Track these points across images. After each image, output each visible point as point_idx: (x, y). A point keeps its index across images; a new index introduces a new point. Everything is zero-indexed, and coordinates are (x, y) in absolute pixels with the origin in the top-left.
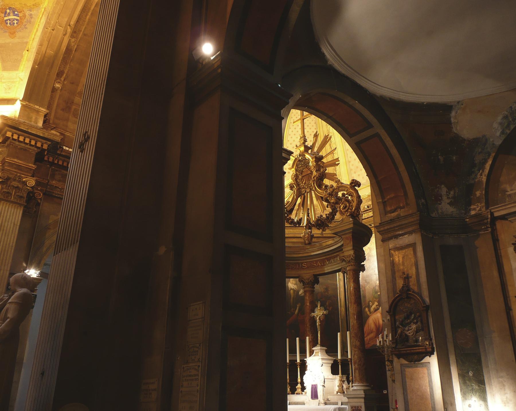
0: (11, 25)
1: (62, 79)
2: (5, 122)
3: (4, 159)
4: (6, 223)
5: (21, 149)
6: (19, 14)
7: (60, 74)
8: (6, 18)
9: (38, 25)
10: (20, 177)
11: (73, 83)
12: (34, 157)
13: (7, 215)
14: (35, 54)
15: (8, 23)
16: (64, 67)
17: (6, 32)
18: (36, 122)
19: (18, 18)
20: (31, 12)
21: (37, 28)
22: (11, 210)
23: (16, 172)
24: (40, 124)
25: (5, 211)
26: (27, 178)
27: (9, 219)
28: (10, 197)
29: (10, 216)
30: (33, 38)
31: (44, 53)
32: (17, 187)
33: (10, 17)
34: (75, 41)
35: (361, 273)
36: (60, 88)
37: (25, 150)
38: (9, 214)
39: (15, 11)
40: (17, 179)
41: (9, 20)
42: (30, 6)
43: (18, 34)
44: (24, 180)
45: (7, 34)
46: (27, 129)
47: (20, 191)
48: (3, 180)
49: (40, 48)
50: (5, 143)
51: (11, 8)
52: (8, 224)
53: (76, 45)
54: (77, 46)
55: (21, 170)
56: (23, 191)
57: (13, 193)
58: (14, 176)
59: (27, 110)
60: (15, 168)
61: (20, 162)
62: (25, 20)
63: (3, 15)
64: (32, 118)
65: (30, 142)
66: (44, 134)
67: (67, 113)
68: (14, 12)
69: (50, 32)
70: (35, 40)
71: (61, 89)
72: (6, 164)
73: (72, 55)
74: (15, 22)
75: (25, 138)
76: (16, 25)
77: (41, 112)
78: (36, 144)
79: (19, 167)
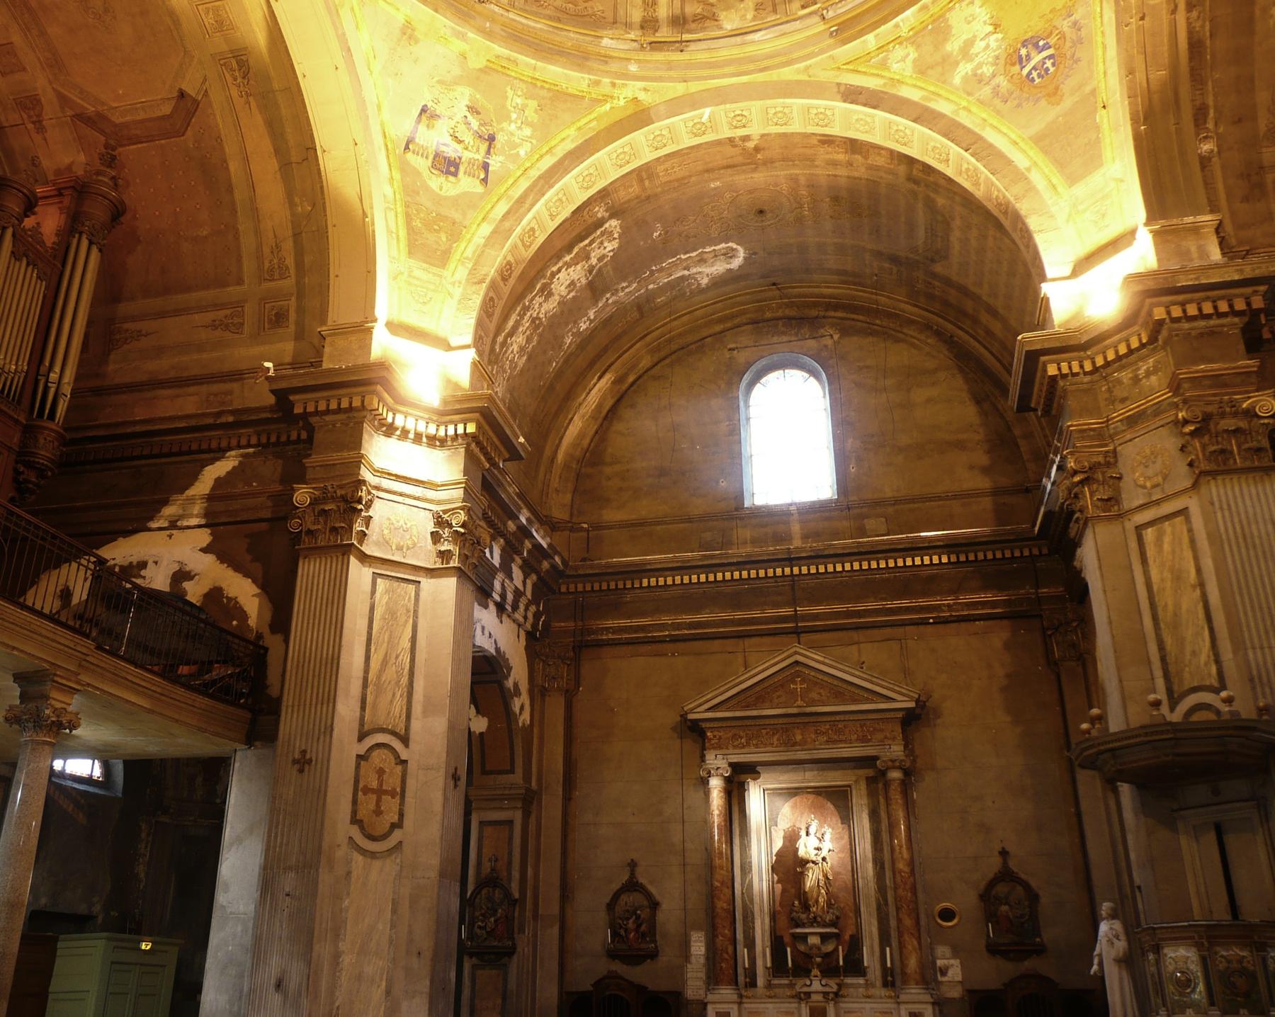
0: (1043, 77)
1: (1210, 125)
2: (1140, 288)
3: (1174, 375)
4: (1254, 527)
5: (1201, 335)
6: (1049, 40)
7: (1200, 115)
8: (1025, 71)
9: (1100, 34)
10: (1233, 404)
11: (1240, 120)
12: (1242, 341)
13: (1245, 507)
14: (1127, 102)
15: (1036, 78)
16: (1202, 94)
17: (1038, 100)
18: (1203, 253)
19: (1050, 51)
20: (1073, 18)
21: (410, 926)
22: (1250, 491)
23: (1214, 395)
24: (1216, 255)
25: (1235, 497)
26: (1249, 398)
27: (1255, 514)
28: (1231, 461)
29: (1254, 507)
30: (1102, 71)
31: (1145, 85)
32: (1237, 431)
33: (1032, 63)
34: (1200, 13)
35: (188, 598)
36: (1216, 149)
37: (1211, 333)
38: (1248, 502)
39: (1038, 42)
40: (1228, 410)
41: (1034, 68)
42: (1064, 7)
43: (1066, 88)
44: (1245, 405)
45: (1043, 103)
46: (1197, 279)
47: (1249, 436)
48: (1198, 426)
49: (1131, 81)
50: (1156, 340)
51: (1026, 41)
52: (1259, 530)
53: (1207, 23)
54: (1211, 21)
55: (1226, 385)
56: (1254, 434)
57: (1235, 448)
58: (1216, 406)
59: (1169, 238)
60: (1211, 387)
61: (1215, 366)
62: (1068, 44)
63: (1017, 67)
64: (1188, 252)
65: (1215, 308)
66: (1241, 271)
67: (1259, 200)
68: (1036, 45)
69: (1138, 28)
70: (1110, 72)
71: (1219, 152)
72: (1186, 386)
73: (1208, 50)
74: (1049, 64)
75: (1199, 304)
76: (1052, 69)
77: (1203, 227)
78: (1231, 306)
79: (1217, 381)
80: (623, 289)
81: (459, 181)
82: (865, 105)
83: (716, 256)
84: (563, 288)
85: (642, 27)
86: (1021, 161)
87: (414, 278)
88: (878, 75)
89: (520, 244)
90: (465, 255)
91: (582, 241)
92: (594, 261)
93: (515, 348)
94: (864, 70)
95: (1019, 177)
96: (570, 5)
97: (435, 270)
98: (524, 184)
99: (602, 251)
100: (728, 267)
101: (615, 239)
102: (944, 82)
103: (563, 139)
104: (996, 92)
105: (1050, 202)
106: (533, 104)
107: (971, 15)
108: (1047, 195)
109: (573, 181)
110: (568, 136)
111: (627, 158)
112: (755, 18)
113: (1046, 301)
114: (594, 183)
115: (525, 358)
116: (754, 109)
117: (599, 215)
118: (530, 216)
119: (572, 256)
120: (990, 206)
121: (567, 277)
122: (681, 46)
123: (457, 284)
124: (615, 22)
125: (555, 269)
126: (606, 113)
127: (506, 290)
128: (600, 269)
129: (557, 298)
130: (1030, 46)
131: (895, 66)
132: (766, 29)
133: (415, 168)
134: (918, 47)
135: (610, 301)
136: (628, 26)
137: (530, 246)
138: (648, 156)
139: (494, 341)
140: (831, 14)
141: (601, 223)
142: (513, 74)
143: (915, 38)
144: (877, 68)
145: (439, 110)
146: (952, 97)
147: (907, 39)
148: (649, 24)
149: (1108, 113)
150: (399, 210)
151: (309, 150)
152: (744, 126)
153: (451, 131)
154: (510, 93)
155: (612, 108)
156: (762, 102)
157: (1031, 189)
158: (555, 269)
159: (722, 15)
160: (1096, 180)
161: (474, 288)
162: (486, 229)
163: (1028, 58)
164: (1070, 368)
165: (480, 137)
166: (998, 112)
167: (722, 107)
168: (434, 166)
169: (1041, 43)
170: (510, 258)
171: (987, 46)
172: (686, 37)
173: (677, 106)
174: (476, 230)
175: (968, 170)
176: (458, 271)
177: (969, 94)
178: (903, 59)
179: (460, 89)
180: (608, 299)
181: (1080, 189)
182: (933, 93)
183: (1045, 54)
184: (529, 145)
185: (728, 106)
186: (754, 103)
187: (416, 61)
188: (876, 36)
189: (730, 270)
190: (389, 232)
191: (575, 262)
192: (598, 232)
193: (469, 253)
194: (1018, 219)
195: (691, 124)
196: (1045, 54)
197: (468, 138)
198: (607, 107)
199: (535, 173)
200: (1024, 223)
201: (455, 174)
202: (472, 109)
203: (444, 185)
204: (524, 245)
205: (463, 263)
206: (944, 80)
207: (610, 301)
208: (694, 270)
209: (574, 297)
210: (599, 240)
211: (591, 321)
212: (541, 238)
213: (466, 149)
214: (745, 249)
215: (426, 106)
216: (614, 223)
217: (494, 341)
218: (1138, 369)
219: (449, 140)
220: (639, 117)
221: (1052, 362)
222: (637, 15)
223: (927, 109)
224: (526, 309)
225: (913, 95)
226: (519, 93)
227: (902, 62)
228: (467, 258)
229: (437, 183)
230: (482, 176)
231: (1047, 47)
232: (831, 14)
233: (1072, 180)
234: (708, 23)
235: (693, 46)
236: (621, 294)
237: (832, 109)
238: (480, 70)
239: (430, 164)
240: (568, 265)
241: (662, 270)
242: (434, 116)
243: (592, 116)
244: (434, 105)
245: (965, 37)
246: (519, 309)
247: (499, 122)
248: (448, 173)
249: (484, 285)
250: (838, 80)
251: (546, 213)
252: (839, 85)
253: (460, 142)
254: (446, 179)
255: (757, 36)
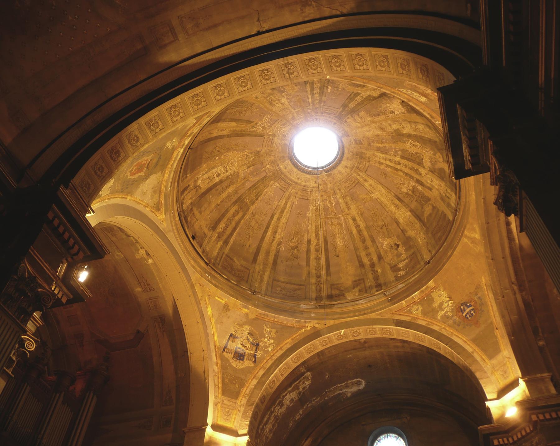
8: (464, 315)
18: (548, 391)
20: (478, 296)
24: (553, 391)
30: (493, 315)
33: (467, 311)
36: (545, 344)
39: (467, 304)
41: (467, 313)
51: (462, 303)
63: (461, 313)
68: (466, 305)
74: (472, 312)
76: (474, 314)
80: (314, 400)
81: (244, 362)
82: (404, 327)
83: (353, 384)
84: (288, 402)
85: (316, 300)
86: (469, 348)
87: (225, 404)
88: (408, 316)
89: (269, 387)
90: (246, 393)
91: (295, 382)
92: (301, 389)
93: (268, 430)
94: (403, 314)
95: (470, 356)
96: (288, 293)
97: (233, 400)
98: (271, 362)
99: (304, 385)
100: (359, 388)
101: (309, 380)
102: (434, 318)
103: (286, 344)
104: (454, 322)
105: (483, 366)
106: (274, 331)
107: (440, 294)
108: (482, 363)
109: (290, 360)
110: (288, 342)
111: (312, 350)
112: (359, 295)
113: (488, 409)
114: (299, 360)
115: (272, 434)
116: (361, 329)
117: (302, 371)
118: (273, 375)
119: (291, 388)
120: (461, 367)
121: (290, 397)
122: (331, 306)
123: (242, 406)
124: (305, 298)
125: (284, 394)
126: (303, 333)
127: (263, 407)
128: (304, 393)
129: (285, 406)
130: (464, 305)
131: (414, 312)
132: (363, 299)
133: (226, 358)
134: (422, 306)
135: (309, 406)
136: (311, 299)
137: (273, 388)
138: (321, 348)
139: (258, 428)
140: (388, 293)
141: (303, 374)
142: (266, 320)
143: (421, 302)
144: (407, 313)
145: (237, 335)
146: (438, 324)
147: (418, 303)
148: (319, 298)
149: (498, 331)
150: (219, 376)
151: (185, 352)
152: (358, 336)
153: (242, 343)
154: (265, 327)
155: (305, 331)
156: (364, 327)
157: (475, 360)
158: (284, 394)
159: (347, 294)
160: (500, 357)
161: (249, 408)
162: (255, 382)
163: (465, 310)
164: (503, 441)
165: (253, 344)
166: (457, 330)
167: (348, 329)
168: (234, 357)
169: (468, 304)
170: (264, 393)
171: (448, 305)
172: (333, 303)
173: (331, 329)
174: (251, 382)
175: (448, 352)
176: (242, 401)
177: (444, 323)
178: (417, 310)
179: (245, 327)
180: (308, 405)
181: (494, 361)
182: (431, 322)
183: (470, 308)
184: (273, 346)
185: (351, 329)
186: (361, 327)
187: (229, 318)
188: (405, 302)
189: (360, 390)
190: (215, 385)
191: (293, 391)
192: (302, 378)
193: (247, 392)
194: (472, 374)
195: (337, 336)
196: (470, 308)
197: (248, 345)
198: (304, 330)
199: (275, 358)
200: (474, 375)
201: (243, 360)
202: (250, 334)
203: (238, 364)
204: (270, 387)
205: (245, 397)
206: (434, 317)
207: (309, 406)
208: (344, 390)
209: (293, 405)
210: (302, 381)
211: (301, 415)
212: (277, 384)
213: (247, 349)
214: (365, 381)
215: (232, 334)
216: (309, 373)
217: (258, 428)
218: (532, 442)
219: (240, 346)
220: (316, 334)
221: (495, 439)
222: (314, 295)
223: (429, 328)
224: (272, 412)
225: (424, 323)
226: (269, 327)
227: (417, 311)
228: (247, 394)
229: (236, 364)
230: (253, 360)
231: (470, 306)
232: (388, 293)
233: (491, 357)
234: (341, 297)
235: (336, 306)
236: (313, 402)
237: (392, 329)
238: (253, 319)
239: (232, 356)
240: (290, 392)
241: (330, 391)
242: (235, 337)
243: (298, 334)
244: (235, 333)
245: (439, 302)
246: (269, 413)
247: (261, 338)
248: (240, 359)
249: (253, 406)
250: (393, 318)
251: (279, 374)
252: (393, 319)
253: (245, 347)
254: (239, 362)
255: (360, 302)
